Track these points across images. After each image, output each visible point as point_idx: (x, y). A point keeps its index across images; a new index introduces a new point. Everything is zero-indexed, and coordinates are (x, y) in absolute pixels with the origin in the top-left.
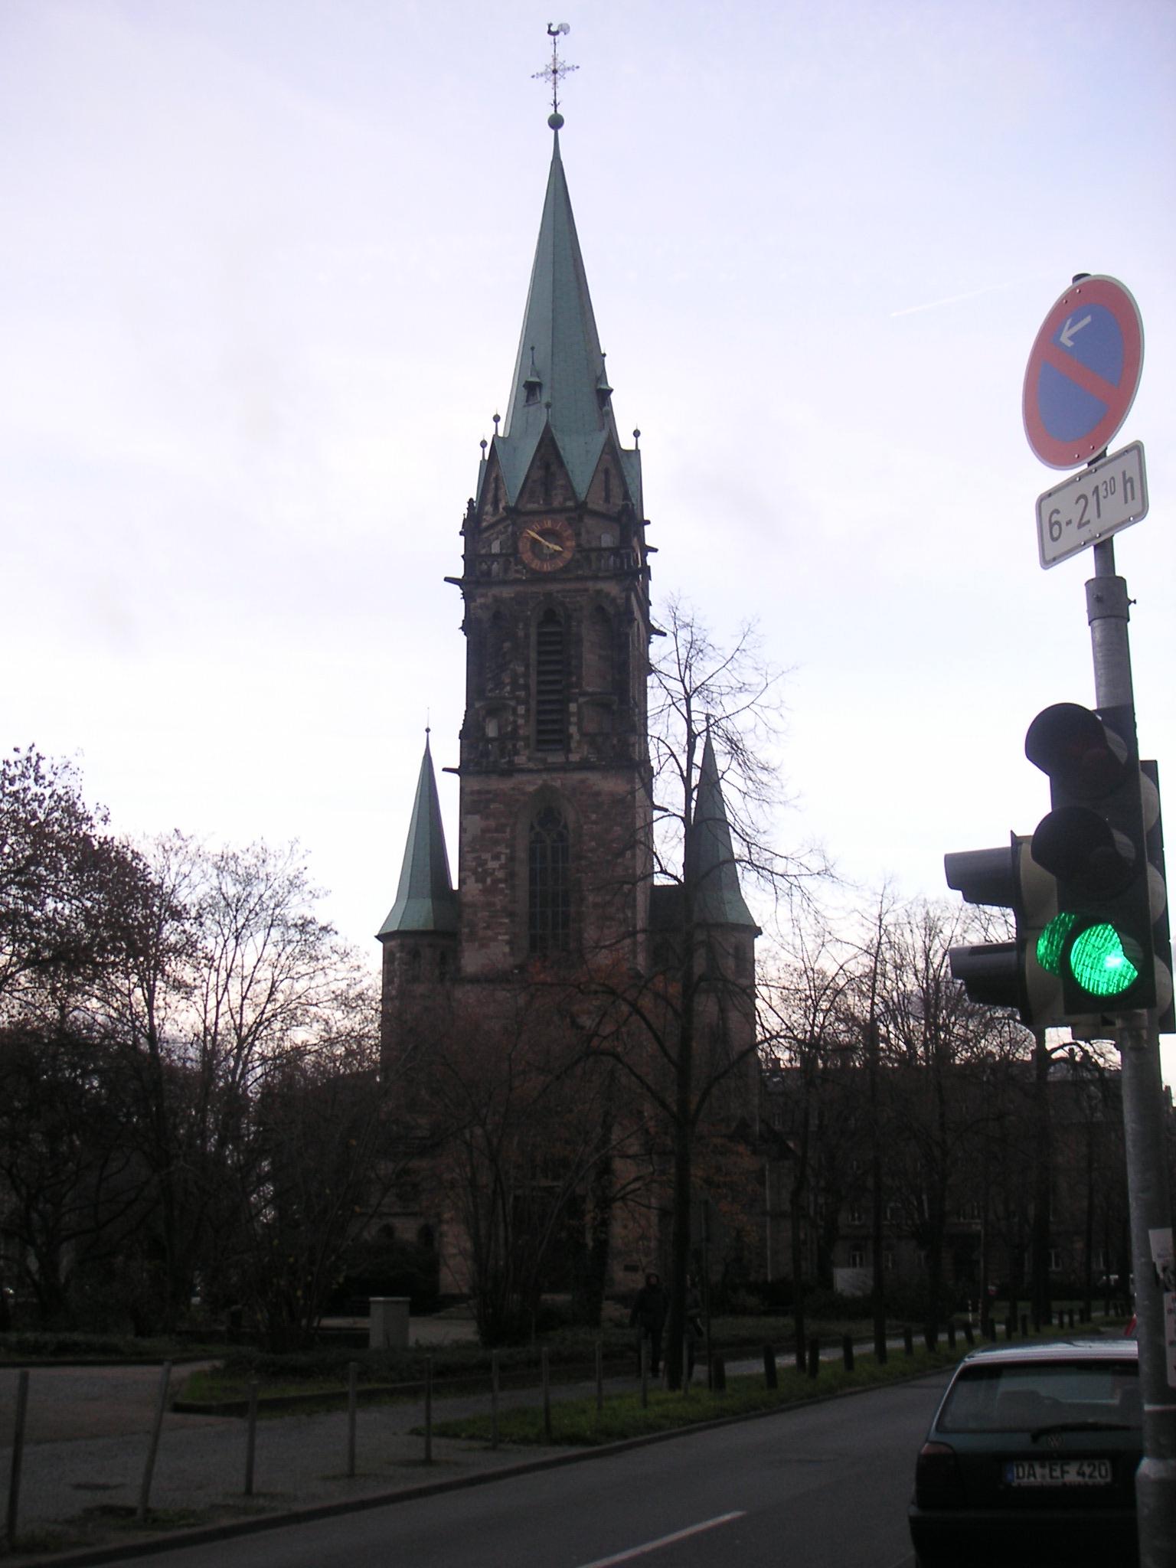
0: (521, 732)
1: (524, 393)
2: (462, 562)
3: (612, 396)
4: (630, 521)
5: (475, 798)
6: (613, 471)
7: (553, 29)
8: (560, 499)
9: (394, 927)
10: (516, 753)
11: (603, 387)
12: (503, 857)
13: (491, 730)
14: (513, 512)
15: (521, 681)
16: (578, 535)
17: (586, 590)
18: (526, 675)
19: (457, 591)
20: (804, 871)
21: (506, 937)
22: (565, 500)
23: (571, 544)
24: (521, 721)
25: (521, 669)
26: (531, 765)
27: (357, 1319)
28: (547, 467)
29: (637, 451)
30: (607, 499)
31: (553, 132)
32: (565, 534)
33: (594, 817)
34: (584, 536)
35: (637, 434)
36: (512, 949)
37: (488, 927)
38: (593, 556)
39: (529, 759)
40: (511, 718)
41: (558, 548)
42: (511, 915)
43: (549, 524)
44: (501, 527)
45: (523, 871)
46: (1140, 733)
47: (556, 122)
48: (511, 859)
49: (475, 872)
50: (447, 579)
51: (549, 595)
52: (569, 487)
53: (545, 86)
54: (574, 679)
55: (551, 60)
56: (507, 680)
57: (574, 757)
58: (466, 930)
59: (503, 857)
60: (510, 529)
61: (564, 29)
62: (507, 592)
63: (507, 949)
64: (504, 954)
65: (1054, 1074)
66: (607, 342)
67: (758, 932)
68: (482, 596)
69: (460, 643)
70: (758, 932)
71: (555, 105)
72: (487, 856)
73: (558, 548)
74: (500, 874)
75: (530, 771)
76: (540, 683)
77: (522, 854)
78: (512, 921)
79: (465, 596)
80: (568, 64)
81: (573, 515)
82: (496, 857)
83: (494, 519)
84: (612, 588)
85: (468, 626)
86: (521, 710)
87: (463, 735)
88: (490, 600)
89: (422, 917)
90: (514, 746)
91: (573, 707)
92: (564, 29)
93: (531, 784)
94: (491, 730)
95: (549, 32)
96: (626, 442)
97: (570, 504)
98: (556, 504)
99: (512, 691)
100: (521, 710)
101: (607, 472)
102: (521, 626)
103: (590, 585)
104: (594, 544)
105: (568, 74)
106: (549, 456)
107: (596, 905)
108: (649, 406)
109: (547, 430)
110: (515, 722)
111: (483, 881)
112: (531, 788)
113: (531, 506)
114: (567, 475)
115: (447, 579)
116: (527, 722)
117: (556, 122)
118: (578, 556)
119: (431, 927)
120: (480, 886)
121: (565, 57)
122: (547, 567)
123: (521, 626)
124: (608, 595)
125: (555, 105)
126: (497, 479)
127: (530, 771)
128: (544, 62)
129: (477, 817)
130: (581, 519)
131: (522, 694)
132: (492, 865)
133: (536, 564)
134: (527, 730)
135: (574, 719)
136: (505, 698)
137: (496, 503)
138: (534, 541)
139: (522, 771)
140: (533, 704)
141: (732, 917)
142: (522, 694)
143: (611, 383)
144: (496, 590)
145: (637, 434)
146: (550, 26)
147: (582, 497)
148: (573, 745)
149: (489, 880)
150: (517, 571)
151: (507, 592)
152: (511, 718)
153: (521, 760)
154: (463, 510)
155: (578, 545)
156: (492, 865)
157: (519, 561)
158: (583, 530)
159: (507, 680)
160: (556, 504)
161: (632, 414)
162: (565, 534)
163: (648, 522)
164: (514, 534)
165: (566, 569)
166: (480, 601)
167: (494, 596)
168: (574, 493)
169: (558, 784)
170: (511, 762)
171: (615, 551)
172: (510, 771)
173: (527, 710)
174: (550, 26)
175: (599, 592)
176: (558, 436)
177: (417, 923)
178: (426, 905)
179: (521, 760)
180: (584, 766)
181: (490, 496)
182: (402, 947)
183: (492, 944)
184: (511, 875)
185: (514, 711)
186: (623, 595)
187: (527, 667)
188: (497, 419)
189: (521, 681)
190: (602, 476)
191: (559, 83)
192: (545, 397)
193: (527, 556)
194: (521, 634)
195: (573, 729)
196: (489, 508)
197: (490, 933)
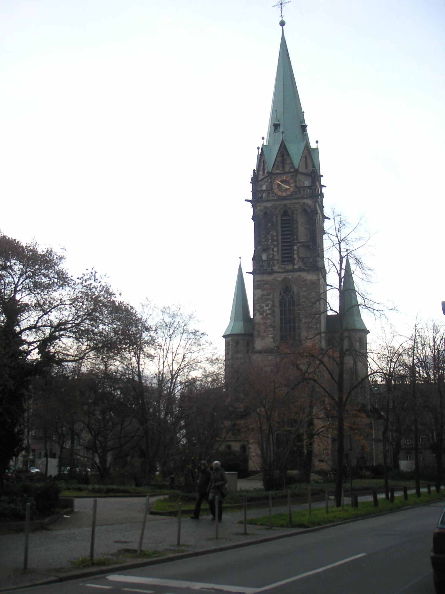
1: (273, 128)
4: (315, 176)
8: (288, 168)
13: (264, 257)
14: (270, 174)
16: (295, 182)
17: (299, 203)
19: (250, 204)
21: (272, 336)
23: (293, 185)
24: (275, 254)
26: (280, 270)
28: (283, 156)
29: (317, 149)
30: (306, 168)
31: (281, 27)
35: (317, 142)
38: (302, 189)
40: (272, 252)
41: (288, 187)
42: (273, 327)
43: (284, 178)
44: (266, 179)
45: (277, 310)
47: (282, 24)
48: (273, 306)
49: (259, 311)
50: (246, 200)
51: (285, 205)
52: (292, 163)
54: (295, 237)
57: (296, 267)
58: (257, 333)
60: (269, 180)
62: (269, 205)
63: (272, 340)
67: (368, 332)
68: (259, 206)
70: (368, 332)
72: (264, 305)
73: (288, 187)
74: (269, 312)
75: (280, 272)
76: (282, 239)
77: (277, 304)
79: (253, 206)
82: (267, 305)
83: (263, 177)
86: (275, 249)
87: (253, 259)
88: (263, 208)
89: (240, 328)
91: (295, 248)
93: (280, 277)
94: (264, 257)
96: (313, 146)
97: (292, 170)
98: (287, 170)
100: (275, 249)
103: (300, 200)
107: (305, 323)
109: (283, 142)
112: (280, 279)
113: (277, 171)
115: (246, 200)
117: (282, 24)
119: (243, 332)
120: (261, 316)
122: (284, 194)
124: (307, 205)
127: (280, 272)
130: (296, 176)
131: (276, 243)
132: (266, 308)
133: (280, 194)
134: (278, 257)
135: (295, 252)
138: (279, 184)
139: (276, 272)
140: (280, 246)
141: (358, 327)
143: (307, 123)
144: (265, 204)
145: (317, 142)
147: (296, 167)
148: (296, 262)
149: (265, 314)
150: (272, 196)
151: (269, 205)
154: (251, 174)
155: (295, 186)
156: (266, 308)
158: (297, 180)
159: (270, 238)
163: (322, 176)
164: (271, 182)
166: (258, 208)
167: (264, 206)
169: (290, 277)
171: (310, 187)
173: (278, 249)
175: (304, 203)
177: (236, 332)
179: (276, 268)
180: (300, 270)
181: (261, 168)
182: (232, 339)
184: (273, 312)
185: (273, 250)
188: (263, 138)
192: (281, 129)
193: (276, 190)
195: (295, 256)
196: (261, 173)
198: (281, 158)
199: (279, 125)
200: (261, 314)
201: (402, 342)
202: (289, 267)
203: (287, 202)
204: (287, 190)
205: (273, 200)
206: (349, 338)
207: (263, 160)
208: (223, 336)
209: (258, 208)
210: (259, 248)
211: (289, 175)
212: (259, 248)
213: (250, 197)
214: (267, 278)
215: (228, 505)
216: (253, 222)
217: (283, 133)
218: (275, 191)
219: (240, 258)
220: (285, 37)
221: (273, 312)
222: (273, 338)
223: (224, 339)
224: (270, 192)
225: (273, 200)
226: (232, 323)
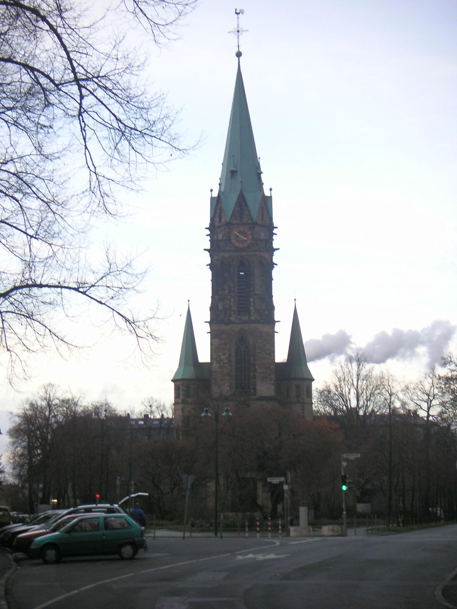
1: (230, 174)
2: (209, 242)
3: (262, 175)
7: (238, 11)
9: (180, 377)
10: (231, 316)
11: (259, 172)
12: (227, 355)
13: (220, 308)
14: (228, 224)
15: (232, 289)
19: (208, 254)
20: (10, 125)
21: (228, 384)
23: (250, 237)
24: (232, 304)
25: (232, 285)
26: (237, 321)
29: (271, 197)
30: (263, 219)
31: (237, 58)
33: (260, 341)
35: (271, 190)
40: (229, 303)
41: (245, 239)
42: (230, 376)
43: (242, 229)
44: (223, 228)
45: (233, 359)
47: (239, 55)
48: (230, 355)
49: (216, 360)
50: (205, 250)
52: (250, 215)
54: (252, 289)
55: (237, 26)
56: (226, 288)
57: (252, 318)
58: (213, 381)
59: (227, 355)
60: (227, 230)
61: (242, 12)
62: (226, 255)
63: (228, 388)
66: (259, 153)
67: (314, 380)
69: (208, 274)
70: (314, 380)
72: (221, 354)
73: (245, 239)
74: (226, 361)
75: (236, 323)
76: (238, 289)
77: (233, 354)
79: (211, 256)
82: (224, 354)
83: (219, 225)
85: (212, 266)
86: (232, 300)
87: (211, 309)
89: (190, 373)
91: (252, 300)
92: (242, 12)
93: (237, 328)
94: (220, 308)
95: (236, 13)
96: (267, 193)
97: (250, 221)
100: (232, 300)
106: (242, 202)
107: (261, 373)
108: (275, 179)
109: (241, 192)
111: (220, 363)
112: (236, 329)
113: (235, 222)
114: (249, 211)
115: (205, 250)
117: (239, 55)
119: (194, 377)
120: (218, 365)
122: (241, 246)
126: (220, 209)
127: (236, 323)
128: (233, 26)
131: (232, 294)
132: (223, 357)
133: (237, 244)
134: (235, 308)
135: (252, 304)
137: (220, 218)
138: (236, 235)
139: (233, 323)
140: (236, 297)
141: (306, 377)
142: (232, 294)
143: (262, 170)
145: (271, 190)
147: (254, 220)
148: (252, 313)
149: (221, 363)
151: (226, 255)
155: (253, 238)
156: (223, 357)
159: (226, 288)
160: (245, 221)
161: (270, 181)
164: (229, 232)
166: (216, 258)
168: (251, 217)
169: (247, 328)
172: (229, 323)
173: (235, 300)
176: (244, 193)
177: (187, 376)
179: (232, 319)
180: (256, 321)
181: (217, 215)
182: (183, 385)
184: (230, 361)
185: (230, 300)
191: (240, 36)
192: (238, 176)
193: (234, 241)
195: (252, 308)
199: (236, 171)
200: (218, 362)
201: (319, 337)
202: (245, 318)
203: (244, 254)
204: (244, 241)
205: (230, 251)
206: (298, 387)
207: (219, 207)
208: (172, 381)
210: (216, 297)
212: (216, 297)
213: (208, 247)
214: (223, 327)
215: (164, 554)
216: (211, 272)
217: (241, 182)
218: (233, 241)
219: (189, 301)
220: (242, 71)
221: (230, 361)
222: (230, 386)
223: (173, 384)
225: (230, 251)
226: (183, 368)
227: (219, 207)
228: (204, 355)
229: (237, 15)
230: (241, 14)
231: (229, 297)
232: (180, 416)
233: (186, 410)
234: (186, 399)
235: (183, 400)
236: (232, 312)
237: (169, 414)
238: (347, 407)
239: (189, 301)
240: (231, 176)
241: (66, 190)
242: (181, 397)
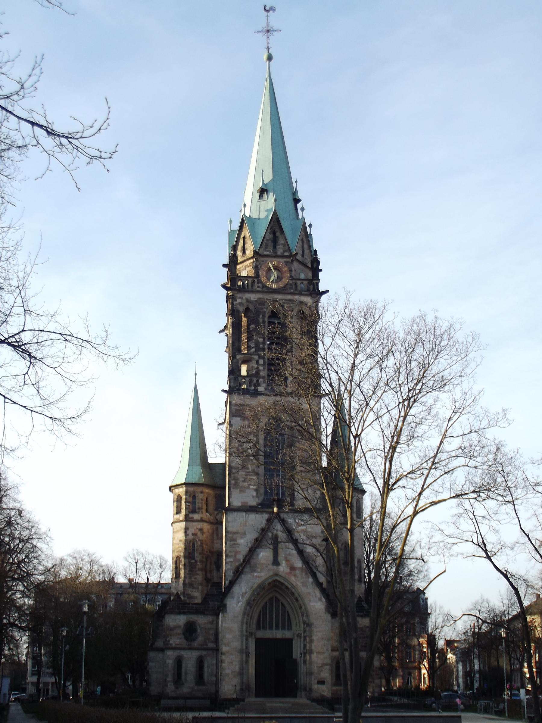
0: (261, 374)
5: (237, 408)
6: (305, 241)
7: (267, 8)
10: (259, 385)
15: (261, 346)
18: (264, 343)
21: (255, 487)
22: (284, 251)
24: (261, 368)
25: (261, 340)
27: (214, 713)
28: (274, 233)
32: (284, 270)
34: (293, 272)
36: (257, 494)
37: (244, 481)
39: (266, 389)
40: (256, 366)
42: (257, 474)
46: (207, 447)
53: (262, 38)
57: (289, 390)
61: (272, 9)
62: (253, 297)
63: (254, 494)
64: (253, 497)
65: (150, 587)
68: (240, 298)
71: (268, 49)
73: (272, 279)
78: (258, 478)
80: (261, 34)
81: (288, 260)
84: (308, 300)
86: (261, 362)
88: (244, 301)
90: (258, 381)
92: (272, 9)
97: (287, 254)
99: (256, 351)
100: (261, 362)
101: (302, 240)
102: (261, 316)
103: (297, 297)
104: (297, 277)
105: (275, 33)
110: (258, 368)
113: (266, 253)
116: (264, 368)
118: (291, 282)
121: (274, 24)
123: (261, 316)
125: (268, 49)
128: (262, 25)
129: (238, 419)
130: (292, 261)
136: (251, 354)
138: (269, 269)
144: (248, 296)
146: (265, 7)
150: (258, 287)
151: (253, 297)
152: (256, 366)
153: (261, 389)
155: (291, 276)
157: (260, 282)
160: (279, 252)
162: (284, 270)
165: (284, 288)
166: (239, 300)
170: (256, 390)
172: (256, 394)
173: (264, 362)
174: (265, 7)
175: (301, 302)
177: (193, 480)
178: (198, 470)
179: (261, 389)
183: (247, 490)
185: (257, 362)
186: (314, 305)
187: (264, 339)
189: (261, 346)
190: (300, 242)
191: (271, 37)
194: (261, 320)
197: (246, 484)
198: (271, 236)
209: (239, 300)
211: (282, 260)
218: (263, 279)
222: (256, 490)
224: (256, 280)
227: (242, 236)
228: (217, 455)
229: (266, 13)
230: (271, 12)
231: (256, 357)
232: (181, 541)
233: (190, 532)
234: (191, 515)
235: (186, 516)
236: (261, 380)
237: (167, 577)
238: (377, 575)
239: (196, 374)
240: (259, 199)
241: (72, 554)
242: (183, 512)
